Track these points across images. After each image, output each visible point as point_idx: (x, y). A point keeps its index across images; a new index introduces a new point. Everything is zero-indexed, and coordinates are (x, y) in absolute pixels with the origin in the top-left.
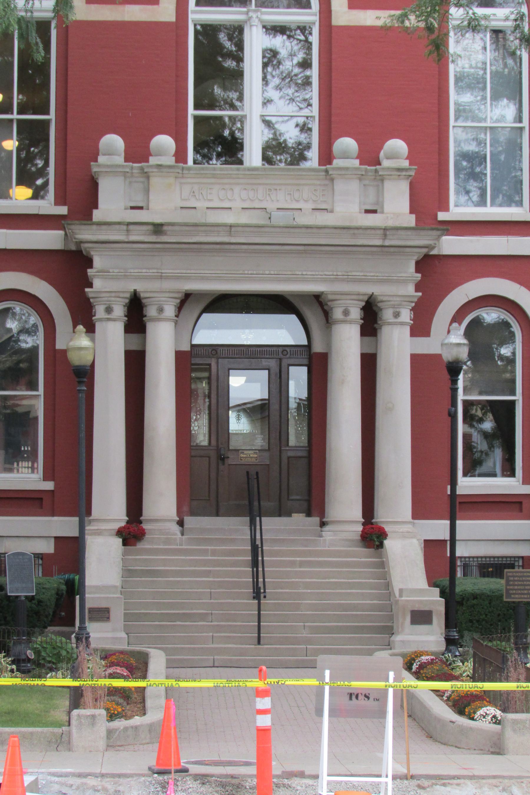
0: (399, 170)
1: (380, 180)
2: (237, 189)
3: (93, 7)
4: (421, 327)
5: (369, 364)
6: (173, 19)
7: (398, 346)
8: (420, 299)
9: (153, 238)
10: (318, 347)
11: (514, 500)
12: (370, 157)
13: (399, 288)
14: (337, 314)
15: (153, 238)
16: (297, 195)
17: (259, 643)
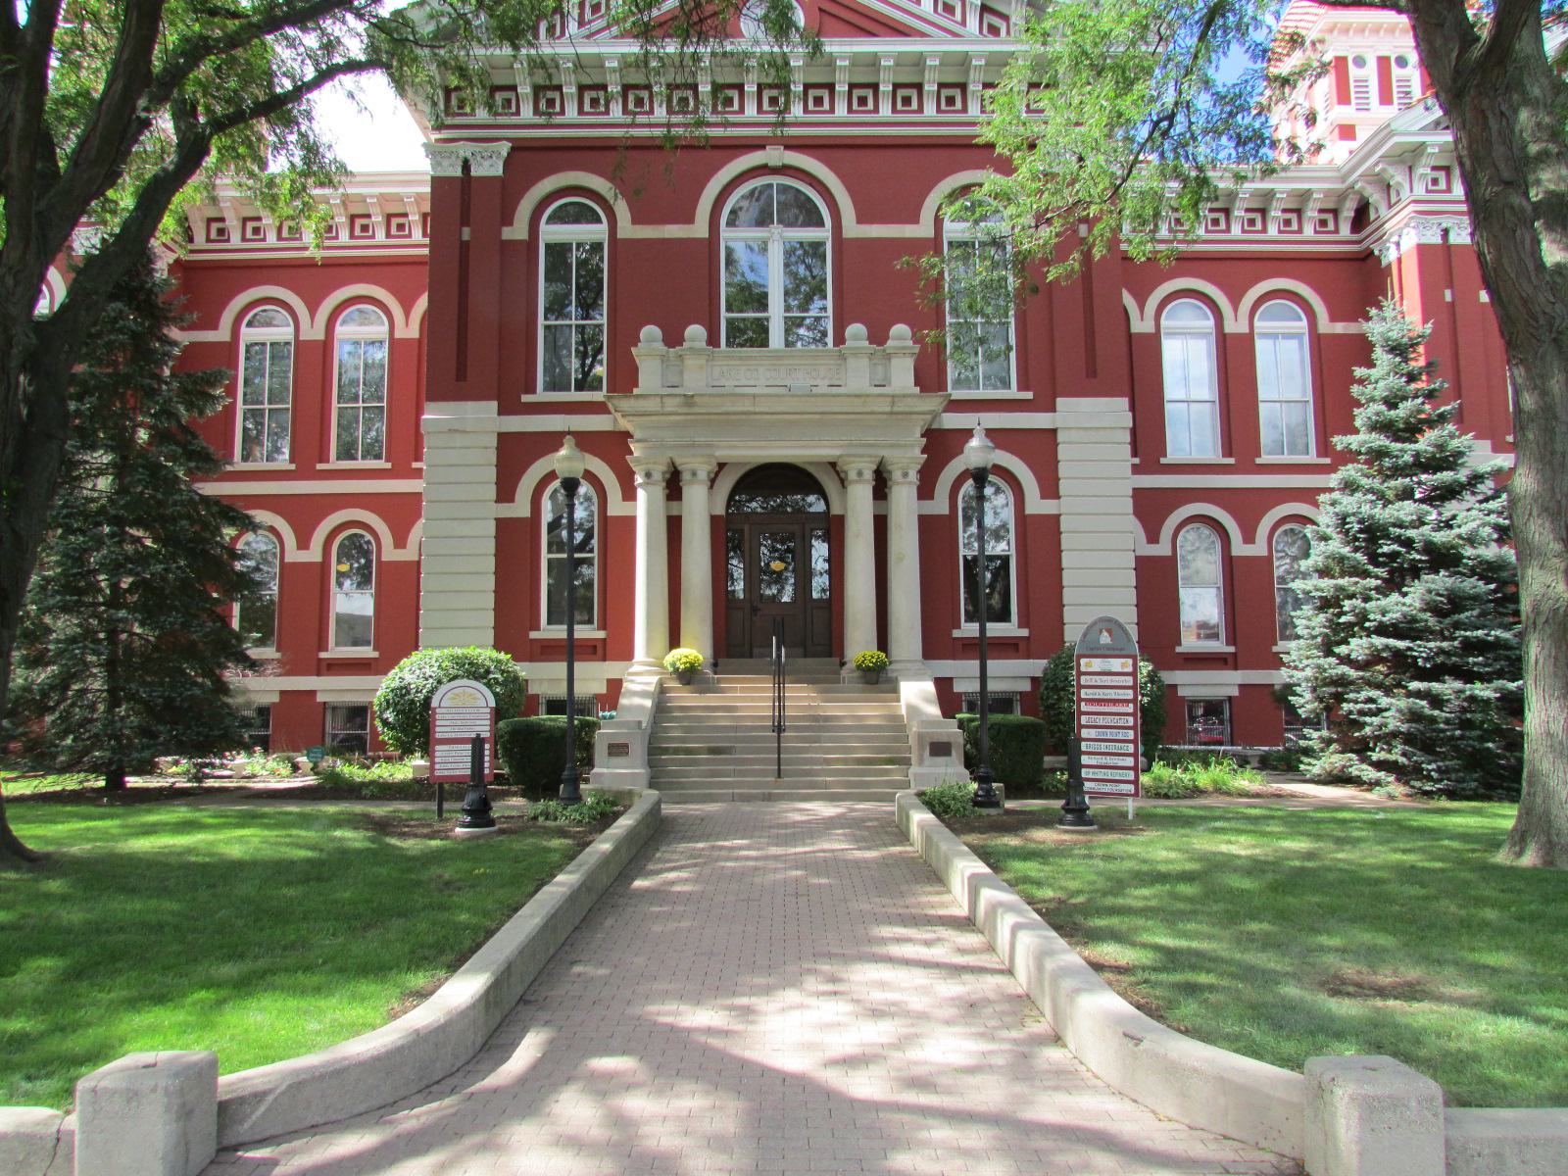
0: (904, 348)
1: (888, 357)
2: (761, 369)
3: (638, 227)
4: (925, 491)
5: (881, 525)
6: (706, 235)
7: (905, 505)
8: (927, 461)
9: (685, 410)
10: (836, 510)
11: (459, 735)
12: (878, 337)
13: (907, 458)
14: (852, 475)
15: (685, 410)
16: (814, 374)
17: (779, 776)
